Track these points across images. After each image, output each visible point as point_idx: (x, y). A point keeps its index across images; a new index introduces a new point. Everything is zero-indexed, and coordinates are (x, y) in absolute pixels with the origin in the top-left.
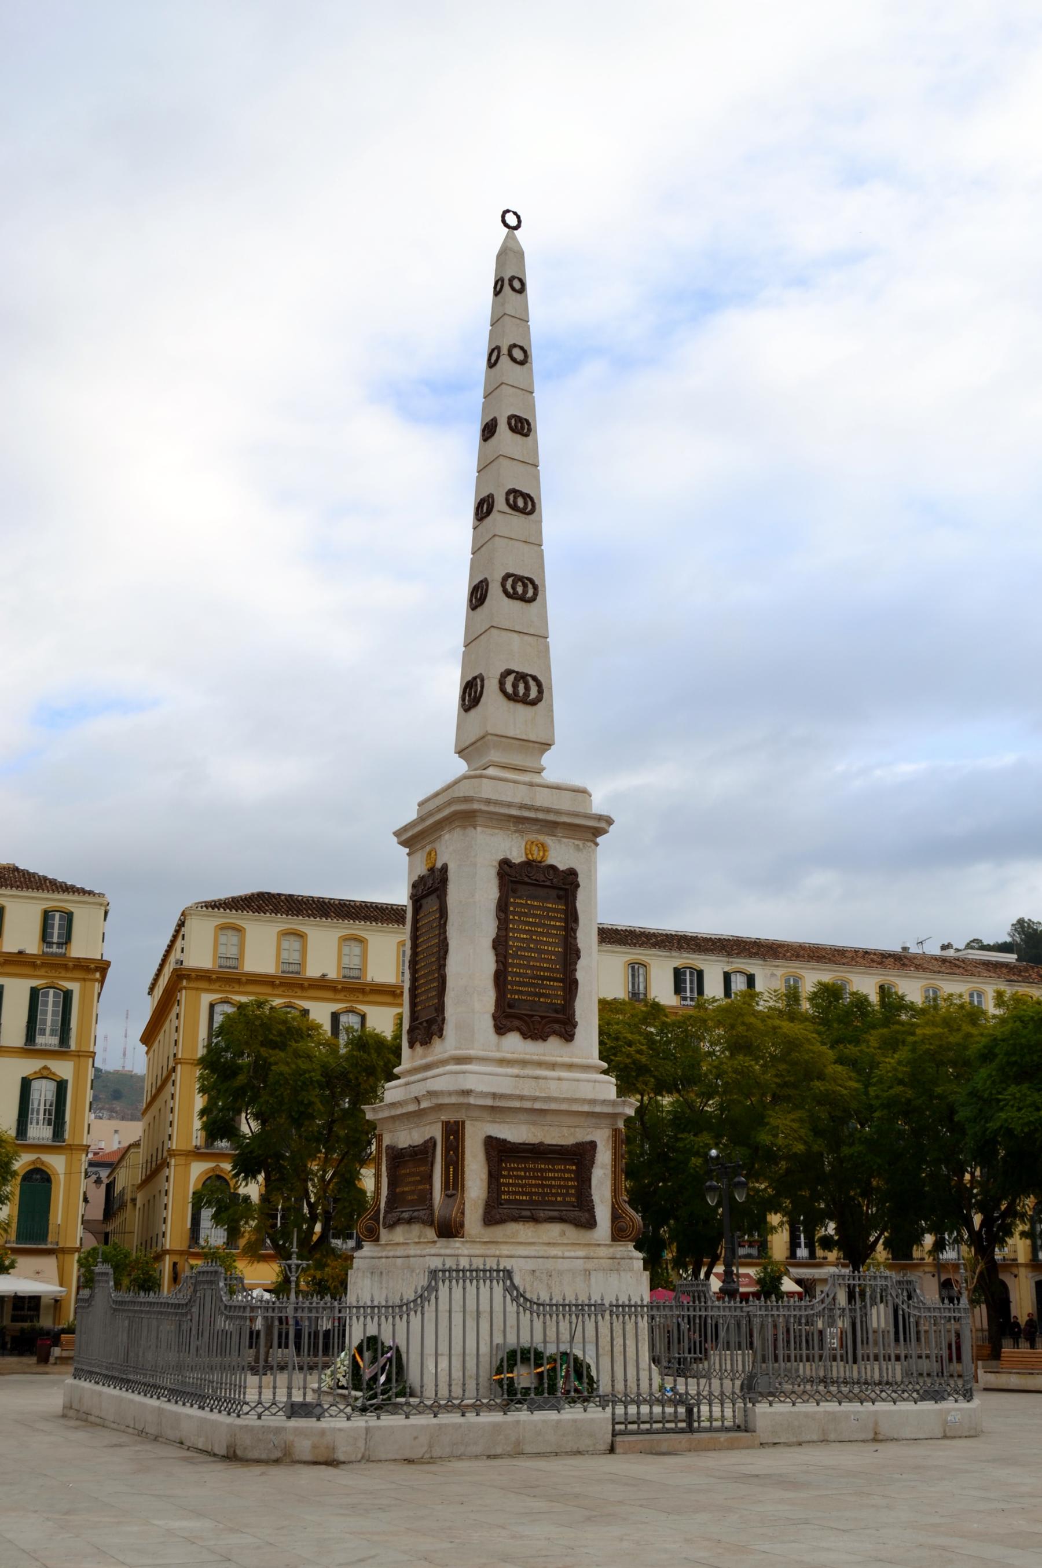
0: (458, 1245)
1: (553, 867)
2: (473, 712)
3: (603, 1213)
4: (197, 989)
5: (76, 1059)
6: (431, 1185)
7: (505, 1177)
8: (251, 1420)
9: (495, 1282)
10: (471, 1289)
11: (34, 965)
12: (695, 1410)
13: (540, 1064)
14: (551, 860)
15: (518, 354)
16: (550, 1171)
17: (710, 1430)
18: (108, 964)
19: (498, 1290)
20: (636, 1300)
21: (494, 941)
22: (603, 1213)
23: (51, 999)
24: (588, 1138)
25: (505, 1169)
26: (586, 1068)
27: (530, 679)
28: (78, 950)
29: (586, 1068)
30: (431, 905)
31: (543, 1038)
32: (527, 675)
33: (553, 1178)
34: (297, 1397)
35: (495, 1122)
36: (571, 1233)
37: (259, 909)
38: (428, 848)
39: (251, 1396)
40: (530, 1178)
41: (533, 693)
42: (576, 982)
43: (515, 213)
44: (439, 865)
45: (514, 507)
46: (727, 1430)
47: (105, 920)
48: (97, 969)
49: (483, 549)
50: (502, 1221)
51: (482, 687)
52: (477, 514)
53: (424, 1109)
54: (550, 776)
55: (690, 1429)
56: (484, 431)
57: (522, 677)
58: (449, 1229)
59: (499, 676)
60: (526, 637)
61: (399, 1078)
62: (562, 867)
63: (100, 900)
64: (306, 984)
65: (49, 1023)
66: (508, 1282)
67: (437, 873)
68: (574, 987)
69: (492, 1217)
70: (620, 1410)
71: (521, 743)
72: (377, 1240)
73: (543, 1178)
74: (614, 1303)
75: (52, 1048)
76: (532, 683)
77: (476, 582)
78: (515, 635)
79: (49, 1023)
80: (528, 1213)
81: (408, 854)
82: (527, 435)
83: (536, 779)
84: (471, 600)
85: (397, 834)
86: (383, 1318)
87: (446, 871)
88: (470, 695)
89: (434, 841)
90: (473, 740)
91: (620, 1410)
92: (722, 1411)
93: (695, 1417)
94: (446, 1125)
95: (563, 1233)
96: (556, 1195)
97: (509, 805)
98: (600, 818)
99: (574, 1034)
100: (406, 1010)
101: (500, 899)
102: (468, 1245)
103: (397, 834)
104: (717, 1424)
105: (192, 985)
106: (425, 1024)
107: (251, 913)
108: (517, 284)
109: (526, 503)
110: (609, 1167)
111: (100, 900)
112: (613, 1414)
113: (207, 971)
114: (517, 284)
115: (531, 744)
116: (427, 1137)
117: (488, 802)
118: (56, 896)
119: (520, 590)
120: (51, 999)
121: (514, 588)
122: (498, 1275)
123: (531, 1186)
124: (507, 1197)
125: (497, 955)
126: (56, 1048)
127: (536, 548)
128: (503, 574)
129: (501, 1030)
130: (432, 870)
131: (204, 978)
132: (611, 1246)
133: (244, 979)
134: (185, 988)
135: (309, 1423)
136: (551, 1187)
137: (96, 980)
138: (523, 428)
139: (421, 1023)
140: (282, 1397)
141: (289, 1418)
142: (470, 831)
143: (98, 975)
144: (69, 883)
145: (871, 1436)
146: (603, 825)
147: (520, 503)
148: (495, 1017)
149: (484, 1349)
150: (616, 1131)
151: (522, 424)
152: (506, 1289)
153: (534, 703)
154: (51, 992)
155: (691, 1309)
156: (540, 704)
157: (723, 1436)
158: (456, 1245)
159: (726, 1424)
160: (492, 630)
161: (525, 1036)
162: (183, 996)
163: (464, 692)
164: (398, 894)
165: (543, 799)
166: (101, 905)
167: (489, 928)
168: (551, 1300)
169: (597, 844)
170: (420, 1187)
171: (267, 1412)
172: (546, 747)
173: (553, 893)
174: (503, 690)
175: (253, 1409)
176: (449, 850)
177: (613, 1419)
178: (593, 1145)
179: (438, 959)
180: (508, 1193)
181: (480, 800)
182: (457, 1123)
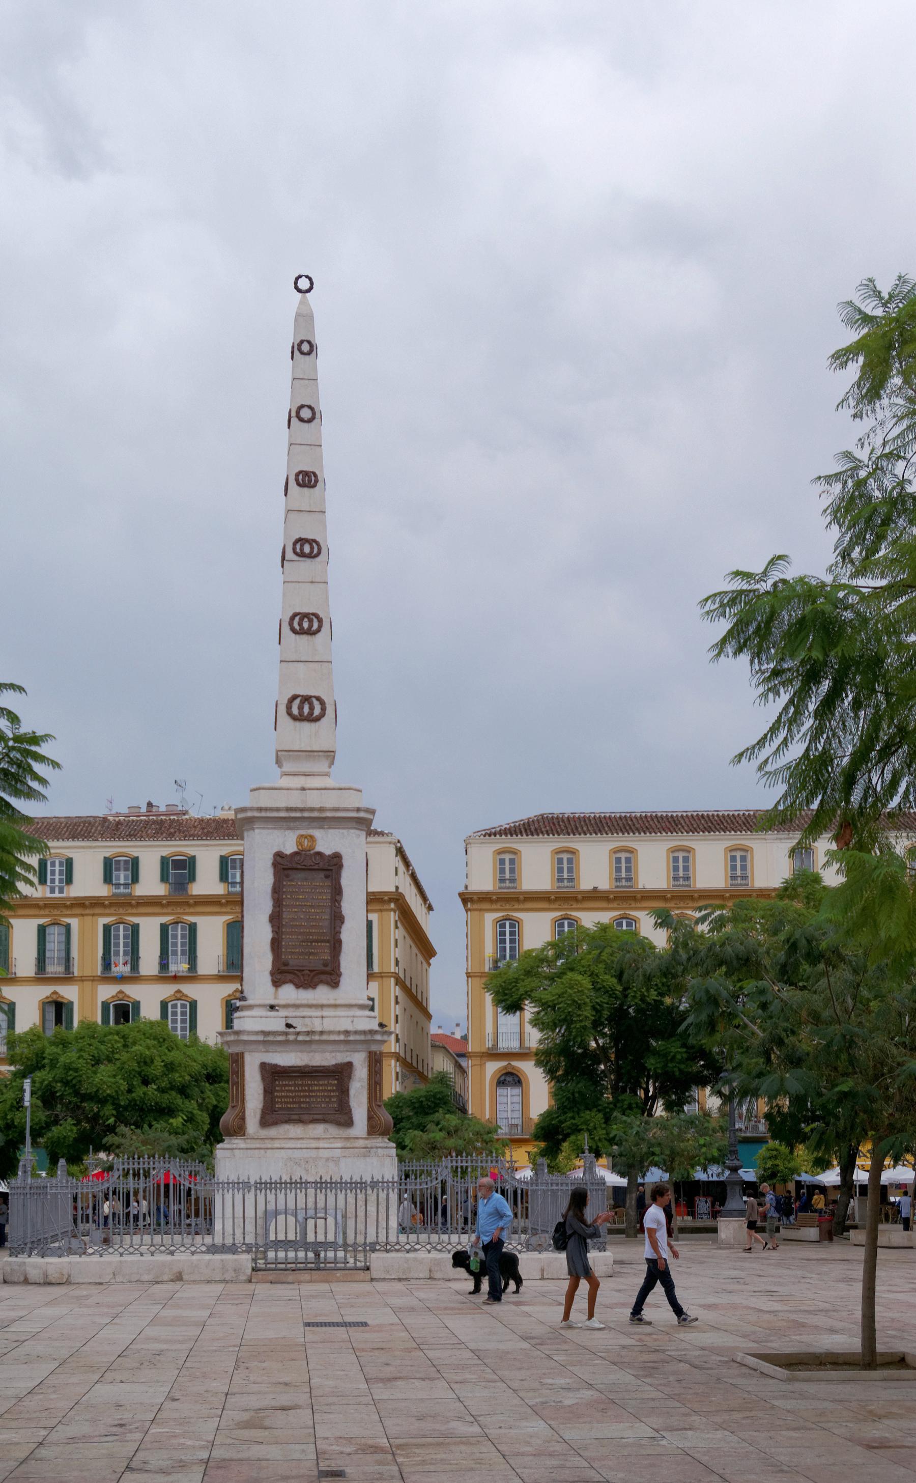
0: (236, 1141)
4: (480, 910)
5: (380, 979)
7: (278, 1091)
13: (310, 1006)
21: (270, 917)
25: (278, 1086)
27: (314, 700)
31: (314, 987)
32: (311, 697)
33: (319, 1091)
36: (333, 1130)
41: (317, 711)
42: (340, 942)
45: (302, 555)
50: (275, 1123)
57: (307, 699)
62: (328, 852)
63: (389, 839)
64: (580, 896)
68: (337, 945)
69: (265, 1122)
74: (258, 1181)
76: (316, 703)
86: (390, 1190)
95: (326, 1131)
96: (318, 1103)
97: (278, 810)
101: (274, 884)
102: (249, 1141)
105: (475, 906)
109: (312, 548)
111: (389, 839)
113: (488, 893)
123: (301, 1097)
127: (321, 585)
132: (366, 1139)
133: (521, 897)
136: (316, 1096)
138: (310, 481)
145: (22, 1279)
147: (307, 549)
148: (272, 974)
149: (250, 1213)
151: (309, 477)
161: (298, 986)
166: (390, 843)
167: (267, 906)
173: (322, 875)
178: (350, 1065)
180: (281, 1103)
181: (251, 809)
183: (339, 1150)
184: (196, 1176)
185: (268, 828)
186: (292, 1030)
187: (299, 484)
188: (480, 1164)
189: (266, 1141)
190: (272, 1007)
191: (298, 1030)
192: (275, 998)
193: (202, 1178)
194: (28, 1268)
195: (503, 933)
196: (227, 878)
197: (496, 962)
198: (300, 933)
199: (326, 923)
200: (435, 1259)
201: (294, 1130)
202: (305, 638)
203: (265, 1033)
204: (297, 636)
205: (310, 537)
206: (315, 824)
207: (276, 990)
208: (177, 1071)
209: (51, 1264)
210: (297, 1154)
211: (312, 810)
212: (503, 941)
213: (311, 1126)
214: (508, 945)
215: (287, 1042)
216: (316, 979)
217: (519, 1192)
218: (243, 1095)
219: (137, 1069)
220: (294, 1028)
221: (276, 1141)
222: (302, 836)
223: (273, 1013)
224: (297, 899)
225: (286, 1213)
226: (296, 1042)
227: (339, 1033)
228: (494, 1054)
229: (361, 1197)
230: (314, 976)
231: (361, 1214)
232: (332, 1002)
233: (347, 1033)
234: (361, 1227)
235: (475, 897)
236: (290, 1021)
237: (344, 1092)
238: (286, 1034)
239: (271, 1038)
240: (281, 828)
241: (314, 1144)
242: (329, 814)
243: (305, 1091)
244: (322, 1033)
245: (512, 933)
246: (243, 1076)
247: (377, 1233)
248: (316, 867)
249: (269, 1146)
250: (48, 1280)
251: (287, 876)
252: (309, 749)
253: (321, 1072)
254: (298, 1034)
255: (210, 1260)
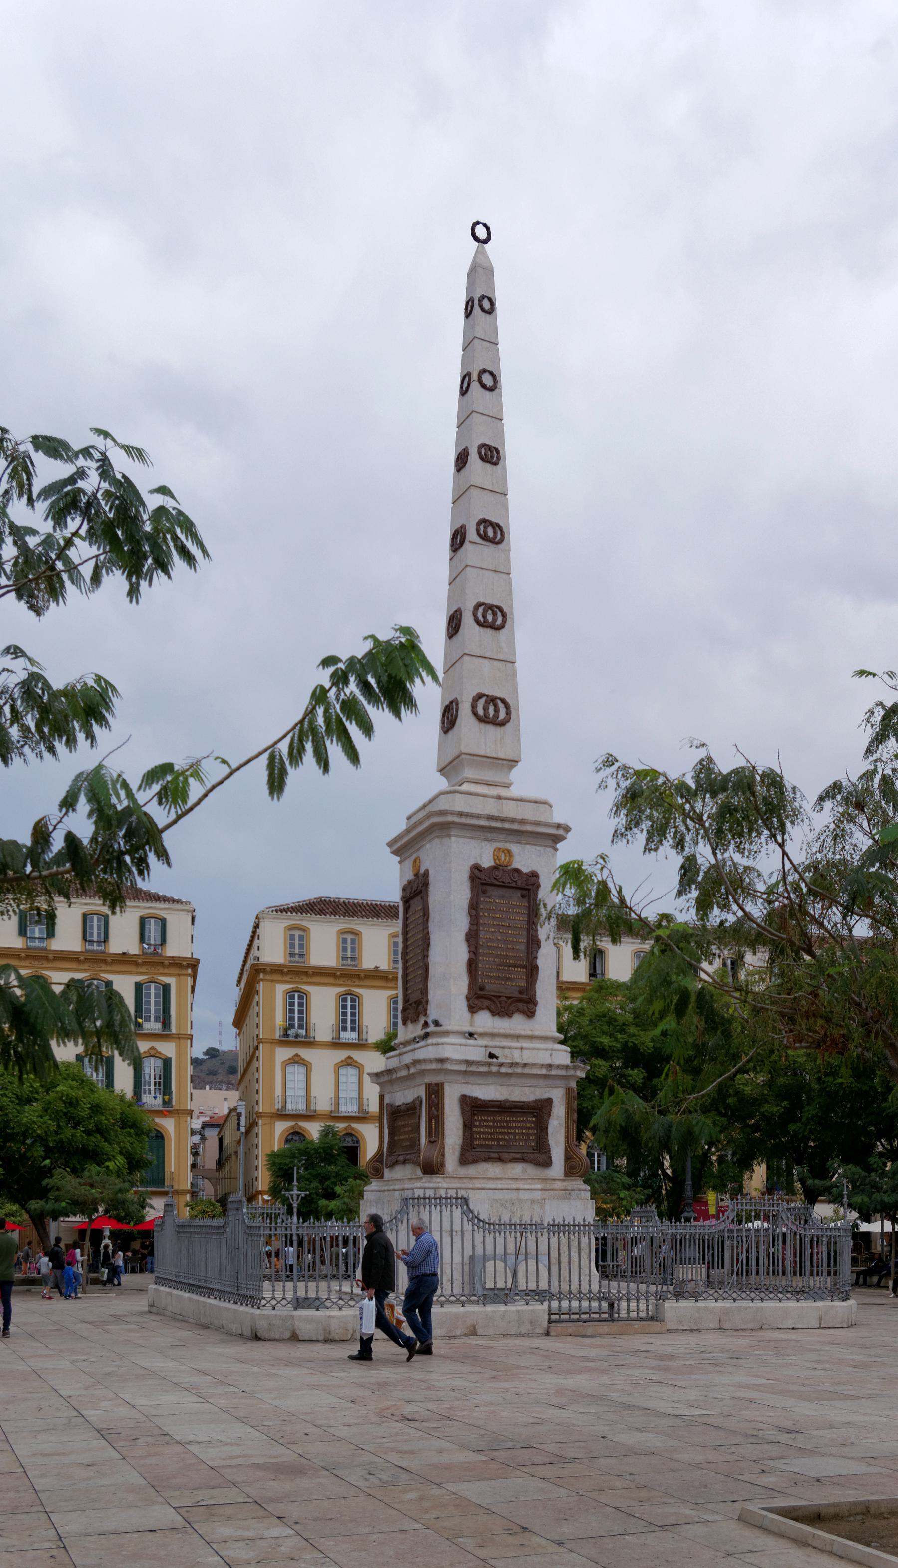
0: (438, 1180)
1: (517, 870)
2: (450, 734)
3: (558, 1153)
4: (272, 981)
6: (419, 1134)
7: (477, 1127)
8: (267, 1311)
9: (454, 1207)
10: (446, 1213)
11: (136, 964)
12: (616, 1305)
13: (506, 1036)
14: (516, 864)
15: (488, 380)
16: (515, 1122)
17: (628, 1319)
18: (198, 961)
19: (458, 1213)
20: (579, 1220)
21: (467, 935)
22: (558, 1153)
23: (153, 992)
24: (546, 1096)
25: (477, 1121)
26: (545, 1038)
28: (173, 950)
29: (545, 1038)
30: (416, 905)
31: (509, 1015)
32: (497, 698)
33: (517, 1128)
34: (301, 1293)
35: (467, 1083)
37: (321, 912)
38: (414, 857)
39: (267, 1295)
40: (498, 1127)
41: (502, 715)
42: (537, 968)
43: (485, 225)
44: (422, 871)
45: (484, 537)
46: (642, 1319)
47: (193, 924)
48: (188, 966)
49: (458, 579)
50: (475, 1162)
51: (457, 711)
52: (452, 545)
53: (413, 1074)
54: (515, 791)
55: (612, 1319)
56: (457, 461)
57: (492, 700)
58: (432, 1169)
59: (471, 700)
60: (496, 662)
61: (395, 1049)
62: (525, 870)
63: (187, 908)
64: (362, 975)
65: (153, 1011)
66: (465, 1207)
67: (420, 877)
69: (465, 1159)
70: (555, 1304)
71: (491, 760)
72: (382, 1177)
73: (508, 1128)
74: (551, 1223)
75: (157, 1032)
76: (501, 705)
77: (452, 612)
78: (486, 661)
79: (153, 1011)
80: (495, 1155)
81: (400, 862)
82: (496, 464)
83: (504, 792)
84: (448, 630)
85: (390, 844)
87: (428, 876)
88: (448, 718)
89: (418, 849)
90: (450, 759)
91: (555, 1304)
92: (638, 1305)
93: (616, 1309)
94: (429, 1086)
96: (517, 1141)
97: (479, 816)
98: (559, 826)
99: (535, 1011)
100: (400, 992)
101: (472, 899)
102: (447, 1180)
103: (390, 844)
104: (633, 1315)
105: (268, 977)
106: (413, 1005)
107: (314, 916)
108: (486, 305)
109: (495, 533)
110: (563, 1119)
111: (187, 908)
112: (550, 1307)
113: (280, 966)
114: (486, 305)
115: (500, 762)
116: (415, 1096)
117: (461, 814)
118: (150, 905)
119: (490, 618)
120: (153, 992)
121: (484, 616)
122: (457, 1202)
123: (499, 1134)
124: (478, 1143)
125: (469, 946)
126: (160, 1032)
127: (504, 576)
128: (474, 603)
129: (473, 1009)
130: (416, 875)
131: (277, 970)
132: (563, 1180)
134: (262, 980)
135: (311, 1312)
136: (515, 1134)
137: (189, 975)
138: (492, 457)
139: (410, 1005)
140: (289, 1295)
141: (296, 1308)
142: (446, 840)
143: (190, 971)
144: (168, 896)
145: (287, 1334)
146: (561, 832)
147: (490, 533)
148: (468, 999)
149: (458, 1259)
150: (569, 1090)
152: (463, 1213)
153: (502, 724)
154: (153, 985)
155: (273, 1229)
156: (508, 725)
157: (637, 1325)
158: (437, 1181)
159: (642, 1315)
160: (466, 658)
161: (494, 1013)
162: (261, 986)
163: (443, 716)
164: (393, 895)
165: (510, 810)
166: (188, 911)
167: (462, 924)
168: (500, 1220)
169: (556, 850)
170: (411, 1136)
171: (279, 1305)
172: (514, 764)
173: (518, 894)
174: (475, 714)
175: (268, 1302)
176: (432, 856)
177: (550, 1310)
178: (549, 1101)
179: (423, 951)
180: (480, 1139)
181: (453, 813)
182: (437, 1084)
183: (540, 1192)
184: (276, 1218)
185: (465, 837)
186: (495, 1060)
187: (481, 458)
188: (745, 1207)
189: (465, 1181)
190: (471, 1035)
191: (501, 1060)
192: (471, 1025)
193: (283, 1221)
194: (297, 1323)
195: (292, 1004)
196: (26, 933)
197: (286, 1030)
198: (498, 956)
199: (523, 948)
200: (725, 1308)
201: (493, 1169)
202: (489, 631)
203: (469, 1063)
204: (482, 629)
205: (494, 520)
206: (511, 838)
207: (472, 1016)
208: (102, 1114)
209: (333, 1317)
210: (499, 1195)
211: (513, 821)
212: (292, 1011)
213: (510, 1166)
214: (296, 1015)
215: (489, 1073)
216: (512, 1008)
217: (815, 1239)
218: (443, 1129)
219: (65, 1110)
220: (497, 1058)
221: (475, 1181)
222: (500, 849)
223: (472, 1042)
224: (495, 918)
225: (495, 1259)
226: (499, 1074)
227: (542, 1066)
228: (282, 1115)
229: (564, 1241)
230: (511, 1004)
231: (565, 1259)
232: (529, 1033)
233: (550, 1066)
234: (565, 1273)
235: (268, 969)
236: (494, 1051)
237: (542, 1129)
238: (490, 1064)
239: (473, 1068)
240: (478, 838)
241: (515, 1186)
242: (529, 828)
243: (504, 1128)
244: (525, 1065)
245: (301, 1004)
246: (443, 1108)
247: (580, 1281)
248: (513, 884)
249: (471, 1186)
250: (331, 1337)
251: (484, 892)
252: (494, 755)
253: (521, 1107)
254: (501, 1065)
255: (506, 1311)
